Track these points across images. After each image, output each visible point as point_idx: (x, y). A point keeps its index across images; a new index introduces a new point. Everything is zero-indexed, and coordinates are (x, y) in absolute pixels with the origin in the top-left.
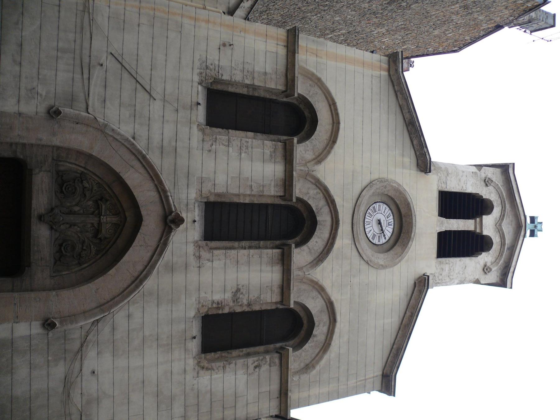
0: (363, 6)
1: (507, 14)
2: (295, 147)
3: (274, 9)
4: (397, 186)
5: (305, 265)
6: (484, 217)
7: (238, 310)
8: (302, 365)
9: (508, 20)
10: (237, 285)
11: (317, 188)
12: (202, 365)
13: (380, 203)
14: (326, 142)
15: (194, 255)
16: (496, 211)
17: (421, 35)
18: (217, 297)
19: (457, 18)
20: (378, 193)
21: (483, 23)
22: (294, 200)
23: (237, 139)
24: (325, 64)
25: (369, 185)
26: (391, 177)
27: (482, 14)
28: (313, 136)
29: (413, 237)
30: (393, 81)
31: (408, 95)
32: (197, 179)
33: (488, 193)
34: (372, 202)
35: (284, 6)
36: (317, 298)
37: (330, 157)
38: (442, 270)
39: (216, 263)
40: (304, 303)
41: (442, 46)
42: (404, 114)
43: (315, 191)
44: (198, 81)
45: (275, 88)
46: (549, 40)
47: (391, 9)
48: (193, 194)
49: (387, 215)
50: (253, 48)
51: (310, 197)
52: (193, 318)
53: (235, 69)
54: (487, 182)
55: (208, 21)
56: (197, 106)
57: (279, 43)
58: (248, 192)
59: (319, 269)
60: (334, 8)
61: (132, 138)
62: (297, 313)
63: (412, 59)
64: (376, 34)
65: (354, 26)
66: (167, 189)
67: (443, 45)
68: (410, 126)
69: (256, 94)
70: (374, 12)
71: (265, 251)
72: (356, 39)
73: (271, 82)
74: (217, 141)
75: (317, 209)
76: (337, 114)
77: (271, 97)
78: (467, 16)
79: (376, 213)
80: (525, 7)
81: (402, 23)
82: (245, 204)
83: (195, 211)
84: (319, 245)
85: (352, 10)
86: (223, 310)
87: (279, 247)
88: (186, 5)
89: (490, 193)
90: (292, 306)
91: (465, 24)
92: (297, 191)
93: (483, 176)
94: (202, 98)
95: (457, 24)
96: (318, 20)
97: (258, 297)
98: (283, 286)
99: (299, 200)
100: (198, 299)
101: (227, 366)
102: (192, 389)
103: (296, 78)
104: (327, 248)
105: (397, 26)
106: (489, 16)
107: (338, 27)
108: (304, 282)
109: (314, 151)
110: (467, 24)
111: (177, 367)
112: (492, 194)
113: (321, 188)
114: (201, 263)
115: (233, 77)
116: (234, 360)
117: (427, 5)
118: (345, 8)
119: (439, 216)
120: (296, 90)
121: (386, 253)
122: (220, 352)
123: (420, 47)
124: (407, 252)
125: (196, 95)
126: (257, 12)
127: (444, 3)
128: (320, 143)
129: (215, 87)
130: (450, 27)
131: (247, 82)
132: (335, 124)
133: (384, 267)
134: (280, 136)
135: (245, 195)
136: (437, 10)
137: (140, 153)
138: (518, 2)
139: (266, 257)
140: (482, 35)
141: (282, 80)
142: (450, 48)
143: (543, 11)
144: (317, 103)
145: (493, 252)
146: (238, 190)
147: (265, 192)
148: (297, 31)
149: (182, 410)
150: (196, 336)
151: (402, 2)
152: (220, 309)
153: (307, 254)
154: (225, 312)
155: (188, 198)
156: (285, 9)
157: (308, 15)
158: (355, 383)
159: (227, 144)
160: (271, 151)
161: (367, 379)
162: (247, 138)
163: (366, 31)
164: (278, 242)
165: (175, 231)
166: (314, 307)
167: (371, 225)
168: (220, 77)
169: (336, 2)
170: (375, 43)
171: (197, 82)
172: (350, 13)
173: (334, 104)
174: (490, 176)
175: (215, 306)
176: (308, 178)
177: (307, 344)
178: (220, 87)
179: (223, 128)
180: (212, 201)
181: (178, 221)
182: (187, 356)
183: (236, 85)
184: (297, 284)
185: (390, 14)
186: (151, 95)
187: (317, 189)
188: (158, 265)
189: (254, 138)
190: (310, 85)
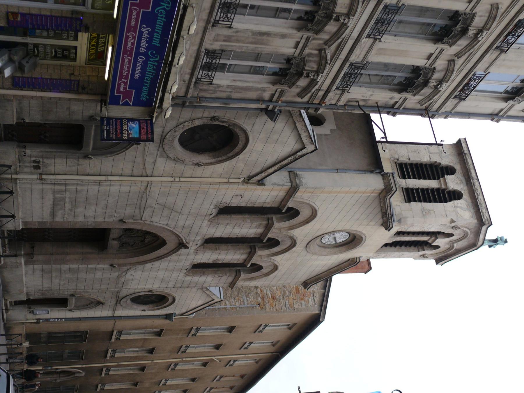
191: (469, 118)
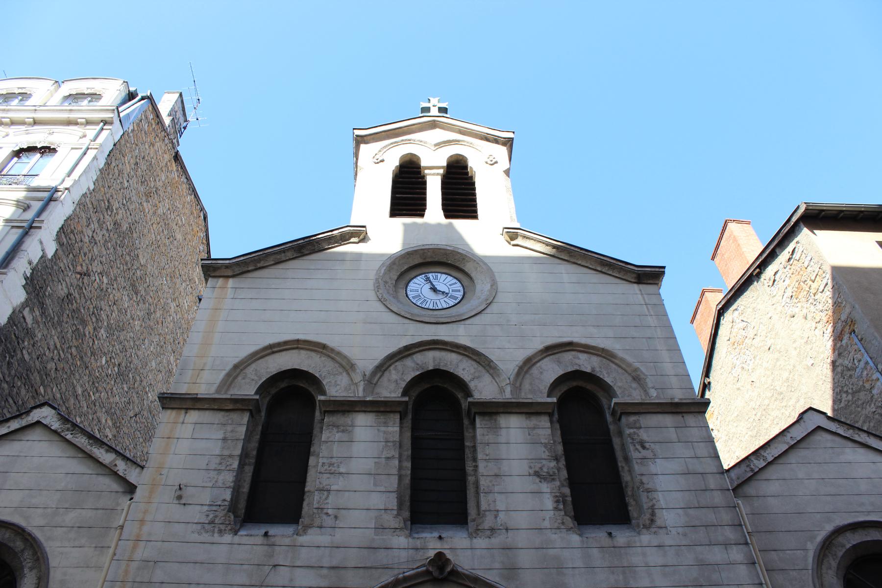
1: (160, 146)
2: (332, 399)
3: (135, 451)
4: (385, 268)
5: (496, 384)
7: (564, 474)
8: (634, 385)
9: (168, 145)
10: (530, 475)
11: (388, 370)
12: (648, 522)
13: (408, 289)
14: (325, 358)
15: (490, 538)
18: (549, 503)
19: (161, 207)
20: (393, 292)
21: (170, 175)
22: (406, 399)
23: (319, 478)
24: (215, 359)
25: (384, 303)
26: (372, 275)
28: (315, 375)
30: (241, 271)
31: (261, 253)
32: (377, 536)
33: (393, 161)
34: (406, 300)
35: (131, 435)
36: (541, 368)
37: (345, 351)
39: (501, 506)
40: (549, 385)
41: (198, 231)
42: (287, 258)
43: (393, 372)
44: (231, 535)
45: (246, 426)
47: (145, 291)
48: (401, 541)
50: (186, 457)
52: (582, 537)
53: (216, 481)
55: (142, 522)
56: (271, 536)
57: (181, 420)
58: (396, 462)
60: (139, 367)
62: (562, 394)
64: (178, 315)
65: (165, 343)
66: (392, 579)
68: (303, 251)
69: (255, 453)
70: (147, 314)
71: (479, 437)
74: (322, 506)
75: (418, 370)
76: (286, 343)
77: (259, 433)
79: (421, 294)
80: (153, 122)
81: (164, 279)
82: (413, 468)
83: (426, 538)
85: (143, 343)
86: (566, 495)
87: (472, 420)
88: (115, 554)
90: (555, 400)
91: (171, 198)
92: (393, 395)
94: (260, 530)
95: (169, 209)
97: (545, 447)
98: (527, 413)
99: (405, 393)
100: (553, 531)
101: (646, 486)
102: (685, 535)
103: (233, 397)
104: (471, 356)
105: (168, 286)
106: (162, 167)
107: (166, 365)
108: (520, 386)
109: (337, 374)
110: (170, 197)
111: (655, 558)
113: (388, 364)
114: (500, 527)
115: (228, 485)
116: (637, 477)
117: (142, 244)
118: (139, 353)
120: (251, 397)
121: (475, 282)
122: (627, 498)
125: (253, 538)
127: (141, 221)
128: (325, 366)
129: (242, 511)
130: (173, 218)
131: (235, 464)
132: (299, 346)
133: (494, 284)
134: (316, 420)
135: (400, 468)
139: (487, 436)
141: (235, 416)
142: (200, 222)
144: (268, 370)
146: (393, 477)
147: (394, 439)
148: (166, 395)
149: (716, 549)
150: (606, 532)
152: (566, 500)
153: (480, 382)
155: (406, 547)
156: (136, 436)
158: (652, 318)
159: (325, 493)
161: (645, 303)
162: (318, 466)
164: (466, 422)
165: (456, 566)
166: (553, 371)
167: (438, 301)
168: (226, 503)
170: (189, 317)
171: (233, 537)
173: (271, 346)
175: (561, 507)
176: (374, 381)
177: (605, 379)
178: (242, 505)
180: (409, 514)
181: (440, 560)
182: (638, 544)
183: (240, 481)
184: (523, 394)
185: (151, 293)
187: (390, 370)
189: (318, 455)
191: (622, 358)
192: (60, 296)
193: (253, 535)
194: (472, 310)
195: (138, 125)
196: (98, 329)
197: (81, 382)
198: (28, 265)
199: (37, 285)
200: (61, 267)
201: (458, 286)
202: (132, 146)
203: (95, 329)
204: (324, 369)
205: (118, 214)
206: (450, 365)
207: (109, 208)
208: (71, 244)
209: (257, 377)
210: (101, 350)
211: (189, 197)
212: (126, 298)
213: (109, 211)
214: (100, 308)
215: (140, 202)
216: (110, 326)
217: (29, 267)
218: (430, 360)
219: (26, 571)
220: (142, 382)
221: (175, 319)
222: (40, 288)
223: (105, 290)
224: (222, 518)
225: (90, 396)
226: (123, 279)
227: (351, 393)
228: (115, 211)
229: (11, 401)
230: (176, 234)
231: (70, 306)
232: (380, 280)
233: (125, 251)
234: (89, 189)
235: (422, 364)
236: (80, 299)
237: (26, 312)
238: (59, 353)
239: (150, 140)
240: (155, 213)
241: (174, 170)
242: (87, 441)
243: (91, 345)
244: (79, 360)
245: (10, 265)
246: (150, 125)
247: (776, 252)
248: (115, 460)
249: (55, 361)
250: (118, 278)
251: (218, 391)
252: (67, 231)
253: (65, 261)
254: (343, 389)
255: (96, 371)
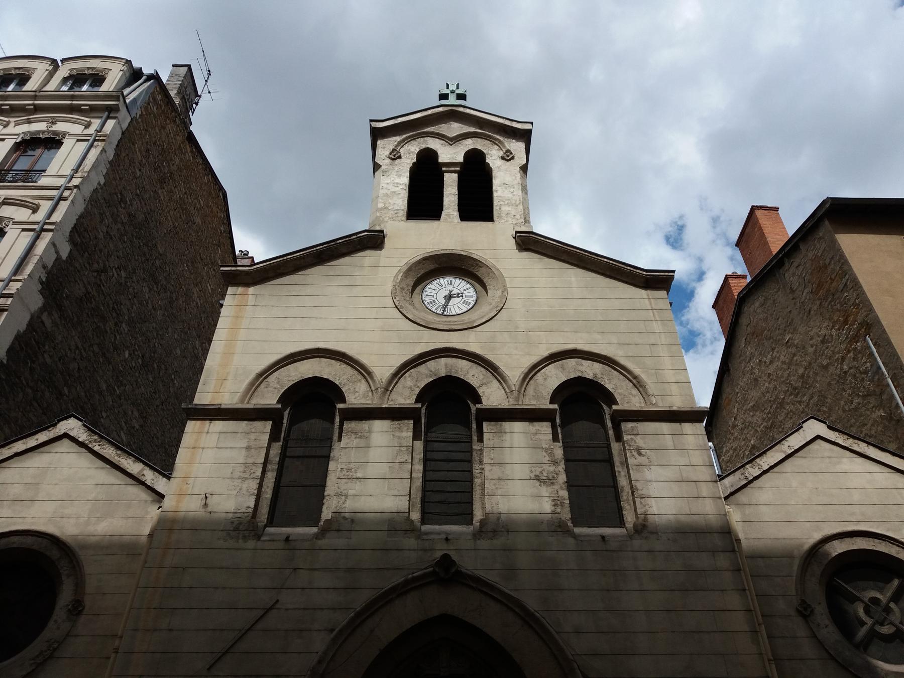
0: (160, 318)
1: (172, 127)
2: (350, 406)
4: (402, 274)
5: (503, 390)
6: (440, 160)
7: (563, 478)
8: (635, 391)
9: (180, 126)
14: (344, 366)
15: (492, 539)
16: (433, 144)
17: (201, 240)
22: (419, 406)
26: (390, 282)
27: (172, 159)
29: (467, 253)
33: (410, 152)
36: (545, 375)
38: (509, 214)
41: (217, 212)
44: (255, 541)
46: (208, 72)
49: (438, 286)
51: (415, 386)
53: (240, 489)
54: (395, 156)
57: (206, 430)
59: (507, 372)
61: (332, 633)
63: (237, 252)
65: (189, 329)
66: (403, 579)
67: (216, 212)
72: (209, 327)
73: (260, 440)
75: (431, 376)
78: (175, 180)
79: (436, 300)
83: (434, 539)
84: (477, 373)
89: (409, 152)
92: (408, 402)
93: (388, 161)
95: (185, 193)
96: (179, 377)
97: (546, 452)
103: (256, 407)
112: (411, 150)
114: (502, 530)
115: (251, 493)
119: (439, 220)
122: (622, 503)
123: (219, 242)
124: (486, 260)
126: (166, 461)
130: (191, 201)
133: (505, 289)
136: (166, 219)
137: (352, 620)
138: (155, 113)
140: (202, 160)
141: (258, 424)
143: (168, 80)
145: (486, 148)
151: (155, 264)
153: (488, 388)
154: (568, 496)
155: (416, 549)
156: (164, 423)
157: (172, 392)
159: (343, 497)
160: (354, 437)
163: (197, 313)
166: (557, 378)
169: (154, 353)
172: (170, 334)
174: (387, 153)
179: (323, 504)
182: (629, 549)
184: (527, 400)
186: (271, 608)
188: (507, 591)
190: (267, 388)
192: (78, 296)
193: (276, 540)
194: (482, 317)
195: (146, 108)
196: (119, 324)
197: (105, 377)
198: (42, 270)
199: (54, 289)
200: (76, 268)
201: (471, 291)
202: (142, 132)
203: (116, 324)
204: (344, 377)
205: (132, 206)
206: (461, 371)
207: (122, 200)
208: (86, 242)
209: (280, 385)
210: (123, 344)
211: (206, 178)
212: (146, 289)
213: (122, 204)
214: (120, 303)
215: (154, 190)
216: (131, 319)
217: (44, 272)
218: (441, 367)
219: (64, 578)
220: (167, 369)
221: (199, 304)
222: (56, 291)
223: (123, 284)
224: (246, 525)
225: (115, 390)
226: (142, 271)
227: (368, 400)
228: (129, 203)
229: (35, 404)
230: (194, 218)
231: (89, 304)
232: (397, 287)
233: (142, 243)
234: (99, 184)
235: (435, 371)
236: (99, 296)
237: (45, 317)
238: (81, 352)
239: (161, 123)
240: (170, 199)
241: (189, 151)
242: (114, 452)
243: (113, 340)
244: (102, 357)
245: (25, 271)
246: (159, 107)
247: (799, 246)
248: (142, 470)
249: (77, 360)
250: (137, 271)
251: (242, 401)
252: (80, 229)
253: (81, 261)
254: (362, 396)
255: (120, 365)
